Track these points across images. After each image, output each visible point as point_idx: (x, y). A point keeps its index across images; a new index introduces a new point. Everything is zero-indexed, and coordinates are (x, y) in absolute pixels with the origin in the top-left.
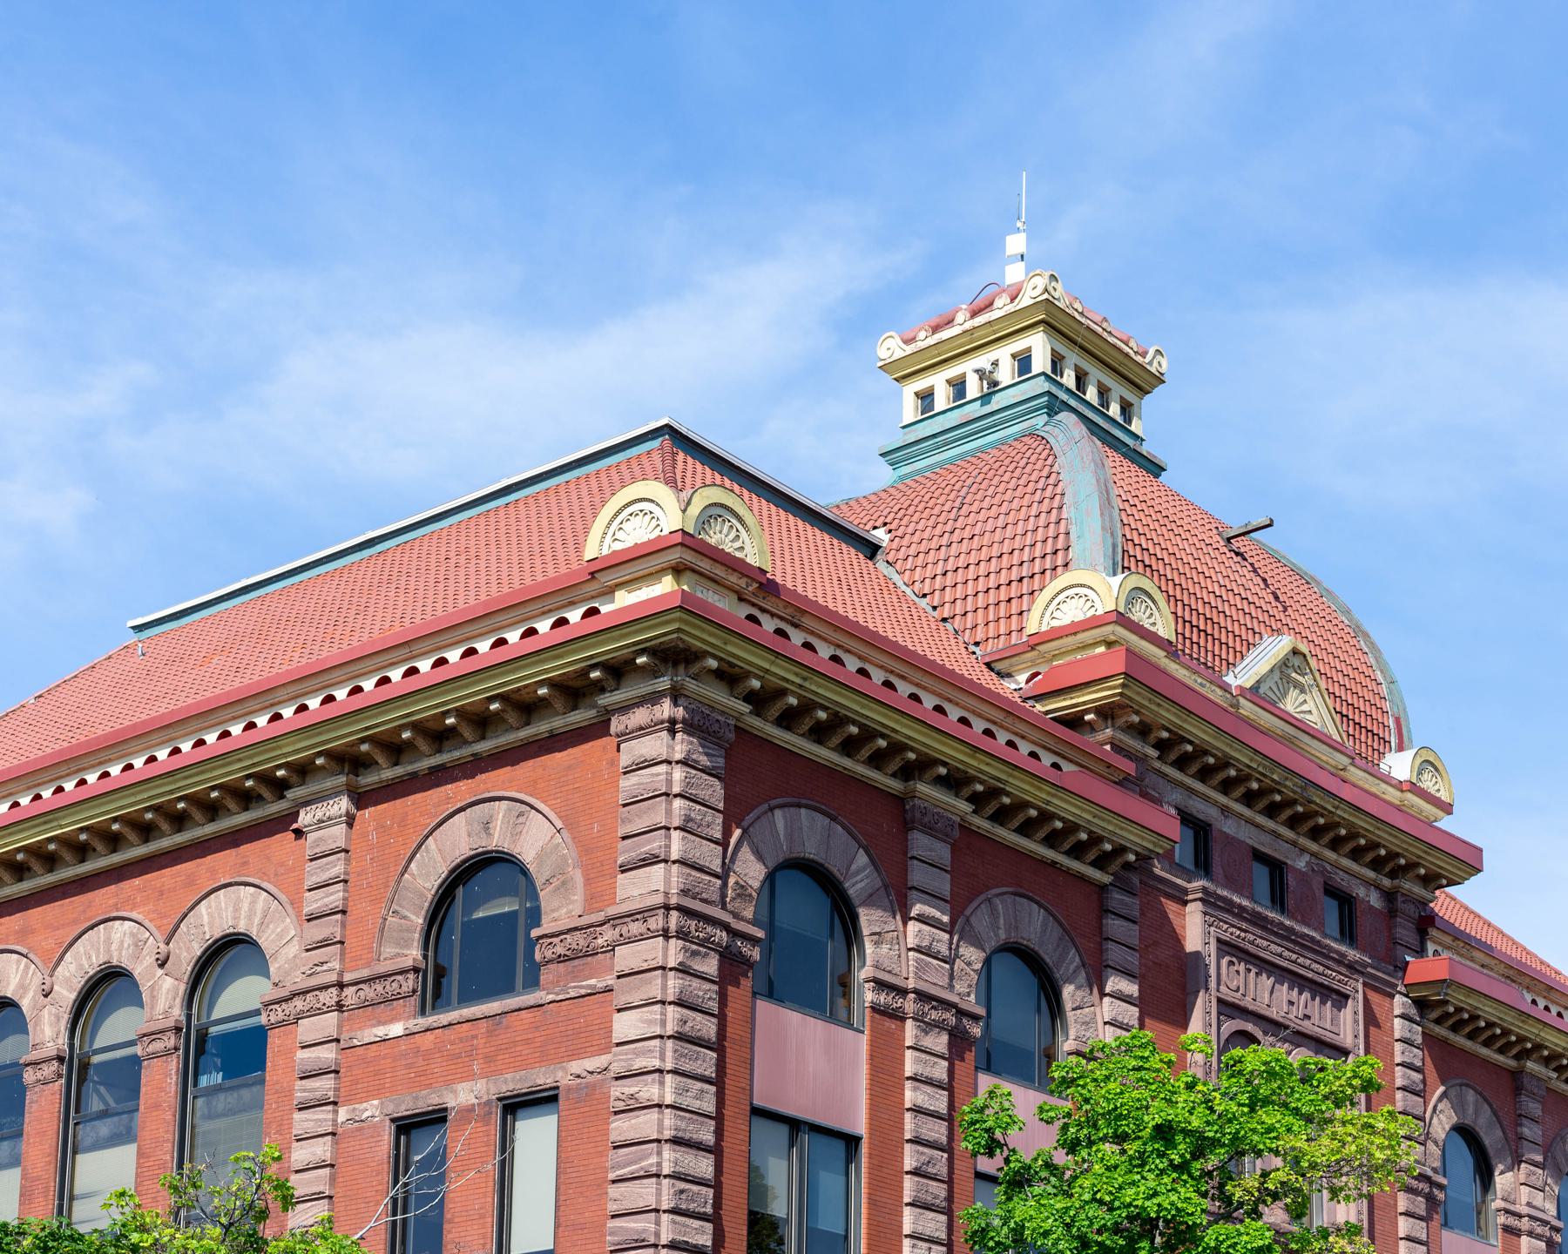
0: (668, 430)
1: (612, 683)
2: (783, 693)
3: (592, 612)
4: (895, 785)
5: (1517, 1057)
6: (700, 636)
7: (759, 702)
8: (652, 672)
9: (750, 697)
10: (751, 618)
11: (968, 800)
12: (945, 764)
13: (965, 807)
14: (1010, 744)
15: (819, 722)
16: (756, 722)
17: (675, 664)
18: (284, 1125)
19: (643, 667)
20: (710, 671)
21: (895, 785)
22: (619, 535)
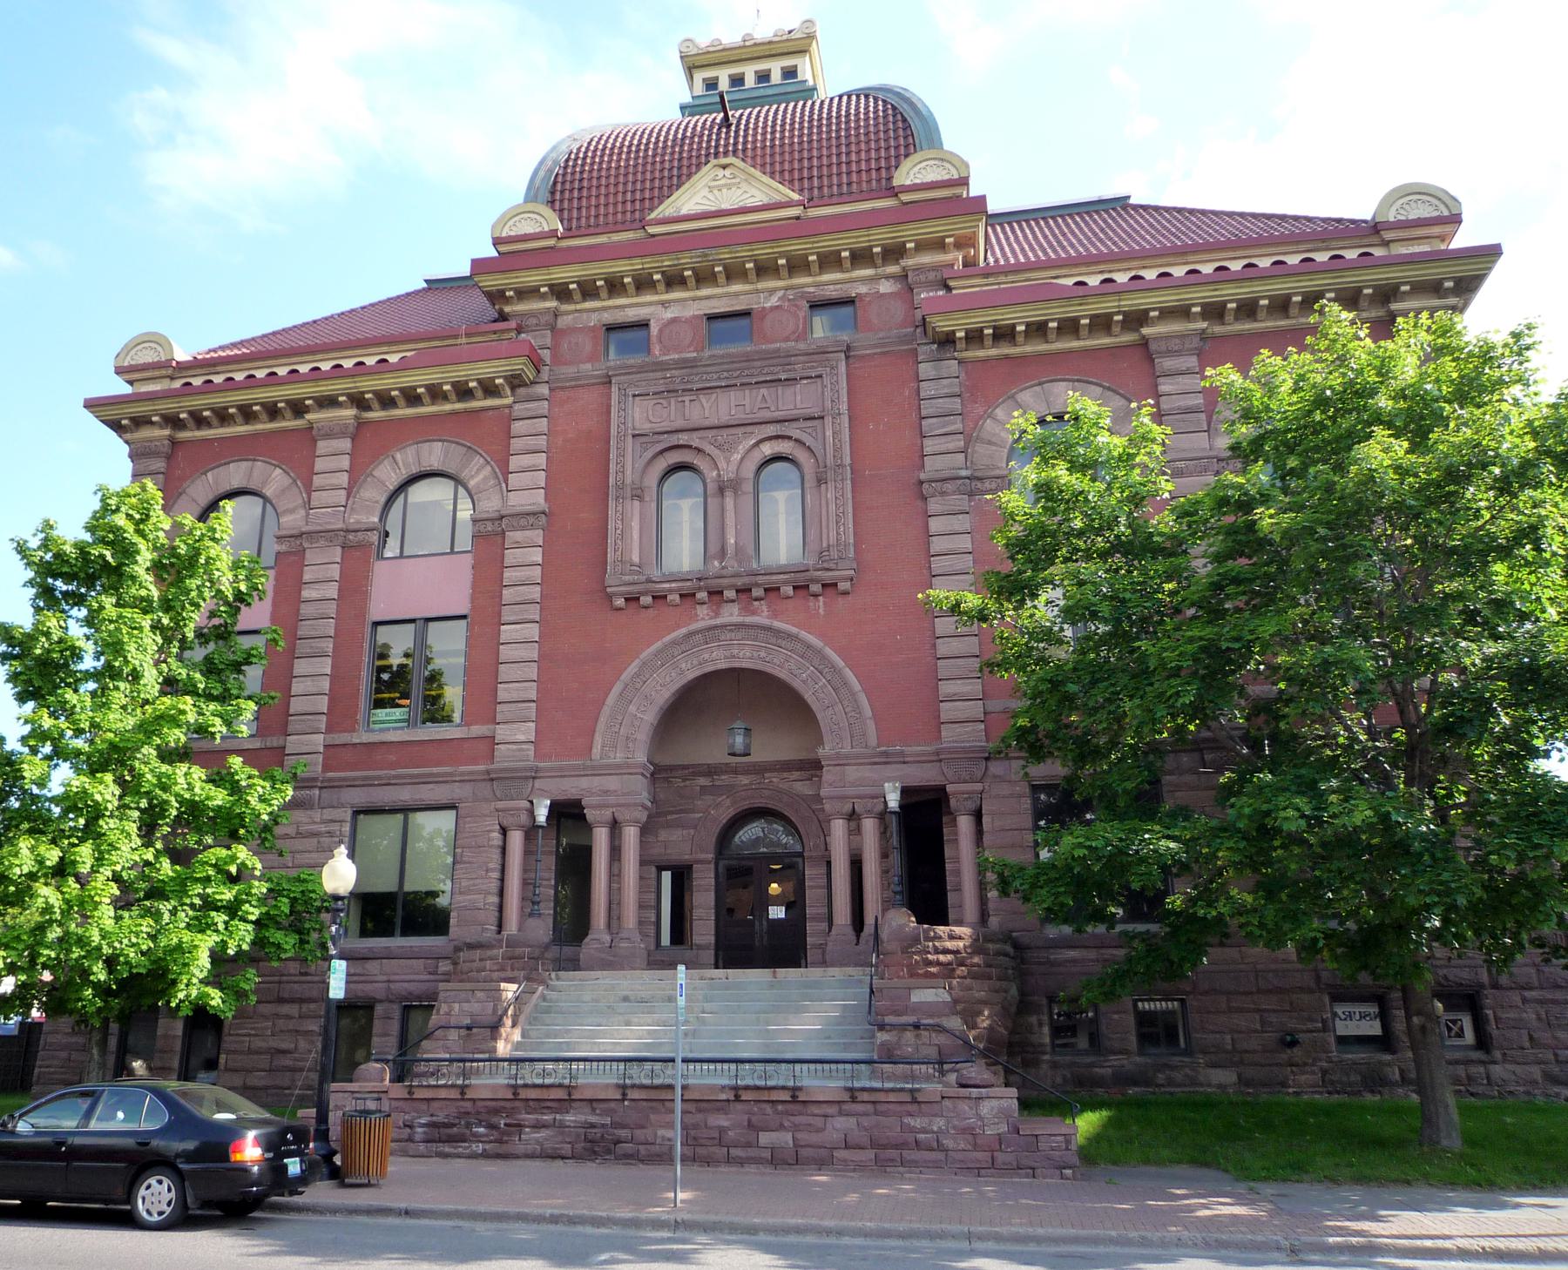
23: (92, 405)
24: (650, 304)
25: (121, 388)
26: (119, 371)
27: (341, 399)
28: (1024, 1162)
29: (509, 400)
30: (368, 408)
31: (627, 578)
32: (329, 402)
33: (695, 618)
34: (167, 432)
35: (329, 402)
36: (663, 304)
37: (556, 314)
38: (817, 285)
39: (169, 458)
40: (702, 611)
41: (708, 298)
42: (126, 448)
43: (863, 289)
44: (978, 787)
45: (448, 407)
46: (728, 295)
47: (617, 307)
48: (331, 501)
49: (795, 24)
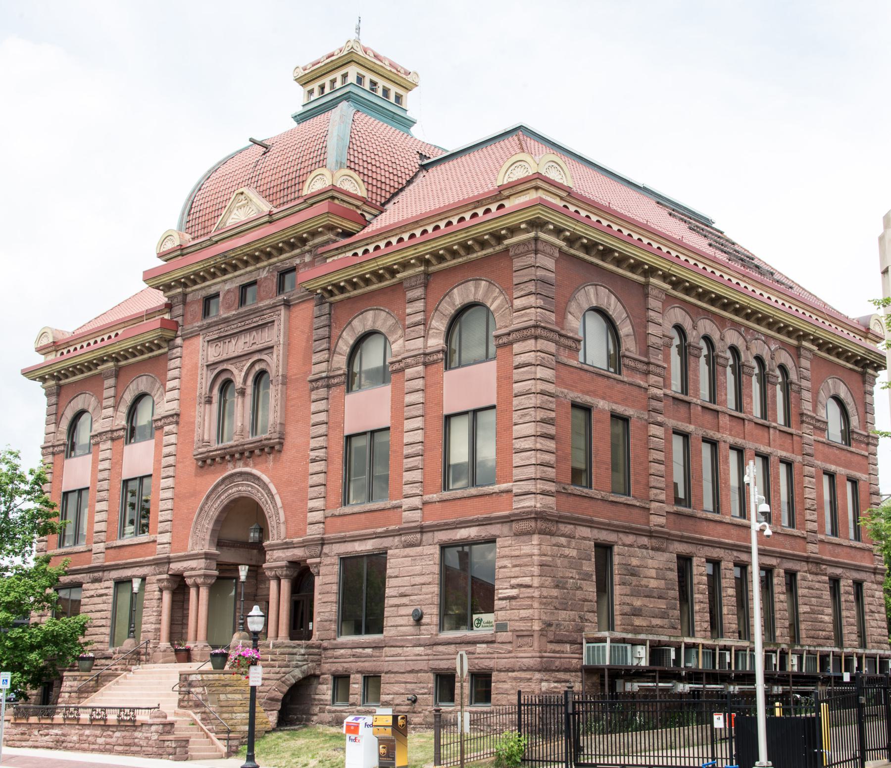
0: (520, 128)
1: (509, 235)
2: (581, 237)
3: (501, 206)
4: (641, 279)
5: (862, 367)
6: (546, 216)
7: (820, 346)
8: (526, 231)
9: (566, 239)
10: (565, 206)
11: (563, 240)
12: (688, 282)
13: (563, 244)
14: (783, 304)
15: (630, 264)
16: (819, 352)
17: (537, 227)
18: (92, 507)
19: (523, 229)
20: (550, 230)
21: (641, 279)
22: (511, 176)
23: (27, 373)
24: (219, 283)
25: (40, 359)
26: (39, 350)
27: (413, 261)
28: (338, 746)
29: (166, 350)
30: (60, 379)
31: (200, 450)
32: (405, 265)
33: (226, 470)
34: (422, 268)
35: (405, 265)
36: (225, 281)
37: (185, 295)
38: (282, 261)
39: (426, 286)
40: (230, 465)
41: (240, 275)
42: (44, 391)
43: (298, 261)
44: (318, 560)
45: (490, 251)
46: (247, 273)
47: (208, 286)
48: (318, 355)
49: (343, 44)
